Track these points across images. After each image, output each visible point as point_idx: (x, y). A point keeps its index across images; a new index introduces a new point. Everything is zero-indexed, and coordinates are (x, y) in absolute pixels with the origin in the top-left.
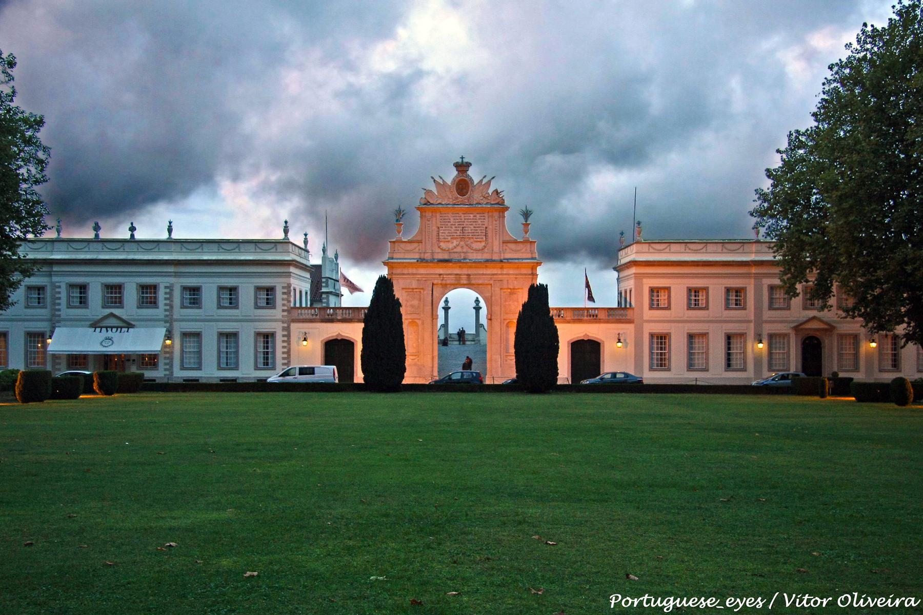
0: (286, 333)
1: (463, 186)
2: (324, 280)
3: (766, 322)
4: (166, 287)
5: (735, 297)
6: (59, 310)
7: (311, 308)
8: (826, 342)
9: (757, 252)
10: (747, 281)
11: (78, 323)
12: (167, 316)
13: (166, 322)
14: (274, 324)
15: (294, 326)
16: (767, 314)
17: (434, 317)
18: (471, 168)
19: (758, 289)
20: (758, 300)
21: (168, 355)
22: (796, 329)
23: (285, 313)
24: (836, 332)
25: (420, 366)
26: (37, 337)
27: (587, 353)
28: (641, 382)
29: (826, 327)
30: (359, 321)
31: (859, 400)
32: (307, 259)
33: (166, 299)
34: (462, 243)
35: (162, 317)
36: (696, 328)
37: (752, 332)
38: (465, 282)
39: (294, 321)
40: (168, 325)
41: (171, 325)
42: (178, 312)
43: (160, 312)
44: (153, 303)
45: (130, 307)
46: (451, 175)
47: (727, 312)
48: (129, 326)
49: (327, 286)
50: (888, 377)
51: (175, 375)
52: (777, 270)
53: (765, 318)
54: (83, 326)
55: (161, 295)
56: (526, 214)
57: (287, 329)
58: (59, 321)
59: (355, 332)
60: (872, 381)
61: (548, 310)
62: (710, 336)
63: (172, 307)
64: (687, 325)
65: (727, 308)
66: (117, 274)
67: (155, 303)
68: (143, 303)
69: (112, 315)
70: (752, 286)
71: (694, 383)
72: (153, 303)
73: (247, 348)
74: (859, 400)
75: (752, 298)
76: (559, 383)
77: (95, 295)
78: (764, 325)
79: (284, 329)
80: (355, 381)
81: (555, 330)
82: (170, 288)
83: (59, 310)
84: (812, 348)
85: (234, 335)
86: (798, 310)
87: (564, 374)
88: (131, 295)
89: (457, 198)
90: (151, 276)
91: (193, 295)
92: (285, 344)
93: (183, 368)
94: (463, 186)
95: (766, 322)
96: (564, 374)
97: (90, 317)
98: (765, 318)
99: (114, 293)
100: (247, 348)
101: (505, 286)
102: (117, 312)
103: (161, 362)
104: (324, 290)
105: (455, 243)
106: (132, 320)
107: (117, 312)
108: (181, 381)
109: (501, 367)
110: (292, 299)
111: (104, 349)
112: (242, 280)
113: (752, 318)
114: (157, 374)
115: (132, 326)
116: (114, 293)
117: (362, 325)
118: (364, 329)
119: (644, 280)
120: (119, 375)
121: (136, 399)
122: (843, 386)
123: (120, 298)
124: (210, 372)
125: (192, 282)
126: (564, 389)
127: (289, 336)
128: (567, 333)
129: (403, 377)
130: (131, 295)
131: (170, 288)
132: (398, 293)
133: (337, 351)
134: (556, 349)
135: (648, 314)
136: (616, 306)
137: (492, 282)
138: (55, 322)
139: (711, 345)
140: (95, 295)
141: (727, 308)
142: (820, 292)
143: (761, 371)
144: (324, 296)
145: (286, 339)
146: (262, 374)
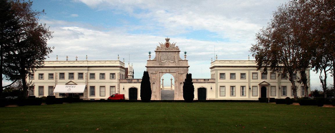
0: (118, 86)
1: (167, 45)
2: (128, 72)
3: (219, 83)
5: (243, 76)
6: (57, 80)
7: (125, 79)
8: (267, 88)
9: (249, 63)
10: (246, 71)
11: (62, 84)
13: (86, 83)
15: (121, 84)
16: (252, 81)
17: (160, 82)
18: (170, 40)
19: (249, 74)
20: (87, 76)
21: (86, 92)
22: (259, 84)
23: (118, 81)
24: (270, 86)
25: (155, 96)
26: (51, 88)
27: (202, 92)
28: (82, 99)
29: (267, 84)
30: (139, 83)
32: (124, 65)
34: (167, 61)
35: (117, 82)
37: (248, 86)
38: (168, 72)
40: (86, 84)
43: (84, 80)
44: (52, 78)
45: (76, 79)
46: (164, 42)
47: (271, 80)
49: (129, 73)
50: (284, 97)
52: (119, 68)
53: (251, 82)
54: (63, 85)
55: (84, 76)
56: (185, 53)
57: (119, 85)
58: (57, 83)
59: (138, 86)
60: (279, 98)
61: (192, 80)
62: (236, 87)
64: (241, 84)
65: (100, 79)
66: (51, 70)
67: (64, 78)
68: (282, 78)
70: (248, 73)
72: (52, 78)
73: (238, 90)
74: (277, 103)
75: (248, 76)
76: (194, 100)
77: (67, 76)
78: (218, 84)
80: (138, 99)
81: (193, 86)
82: (56, 74)
83: (57, 80)
84: (264, 89)
85: (43, 87)
86: (260, 80)
87: (196, 97)
88: (76, 76)
89: (166, 48)
90: (73, 71)
91: (93, 76)
92: (118, 89)
94: (167, 45)
95: (219, 83)
96: (196, 97)
97: (258, 82)
98: (251, 82)
99: (71, 75)
100: (238, 90)
101: (180, 73)
102: (72, 80)
103: (84, 95)
104: (129, 74)
105: (166, 61)
106: (77, 83)
107: (72, 80)
108: (100, 99)
109: (179, 96)
111: (68, 92)
112: (226, 71)
113: (247, 81)
116: (71, 75)
119: (218, 71)
122: (273, 100)
126: (196, 101)
128: (196, 86)
129: (151, 98)
130: (76, 76)
132: (150, 75)
133: (133, 91)
135: (219, 80)
137: (176, 72)
138: (56, 83)
139: (236, 89)
140: (67, 76)
141: (100, 79)
142: (264, 74)
143: (218, 96)
144: (129, 76)
145: (118, 88)
146: (93, 97)
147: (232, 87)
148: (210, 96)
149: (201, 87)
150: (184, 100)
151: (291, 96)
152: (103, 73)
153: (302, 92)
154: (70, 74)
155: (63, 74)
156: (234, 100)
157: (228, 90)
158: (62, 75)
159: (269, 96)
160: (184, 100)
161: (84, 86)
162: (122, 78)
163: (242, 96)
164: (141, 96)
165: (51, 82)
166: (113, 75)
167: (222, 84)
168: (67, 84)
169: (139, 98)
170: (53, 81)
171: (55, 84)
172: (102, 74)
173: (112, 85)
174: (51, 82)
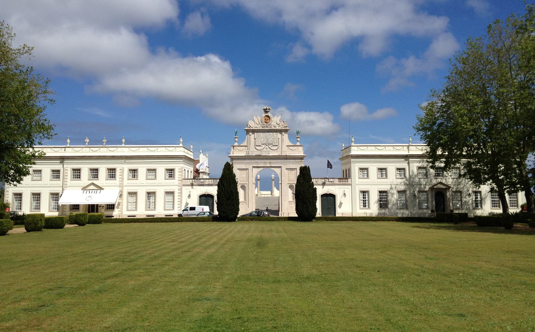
4: (120, 170)
12: (120, 184)
14: (174, 187)
15: (184, 188)
26: (56, 196)
31: (28, 230)
33: (120, 175)
35: (177, 184)
36: (151, 189)
39: (184, 185)
41: (122, 188)
42: (126, 182)
43: (117, 181)
44: (58, 177)
48: (101, 188)
51: (124, 213)
57: (181, 190)
58: (66, 187)
59: (213, 191)
63: (123, 179)
69: (93, 184)
71: (186, 216)
72: (58, 177)
77: (85, 173)
79: (179, 190)
80: (337, 215)
93: (128, 210)
99: (95, 173)
102: (95, 182)
107: (95, 182)
109: (289, 209)
110: (184, 175)
114: (116, 214)
115: (103, 189)
116: (95, 173)
117: (524, 192)
118: (526, 195)
119: (356, 164)
120: (92, 216)
121: (339, 225)
123: (80, 175)
124: (141, 212)
125: (133, 167)
126: (319, 219)
127: (181, 193)
131: (122, 170)
132: (235, 171)
134: (315, 199)
136: (342, 177)
140: (85, 173)
147: (150, 194)
148: (344, 209)
149: (325, 192)
150: (296, 216)
151: (50, 211)
152: (152, 168)
153: (362, 202)
154: (74, 170)
155: (114, 170)
156: (360, 217)
157: (142, 197)
158: (77, 174)
159: (340, 212)
160: (296, 216)
161: (117, 191)
162: (345, 177)
163: (362, 209)
164: (217, 210)
165: (56, 186)
166: (171, 173)
167: (132, 189)
168: (84, 189)
169: (319, 214)
170: (59, 183)
171: (61, 189)
172: (381, 169)
173: (170, 189)
174: (56, 186)
